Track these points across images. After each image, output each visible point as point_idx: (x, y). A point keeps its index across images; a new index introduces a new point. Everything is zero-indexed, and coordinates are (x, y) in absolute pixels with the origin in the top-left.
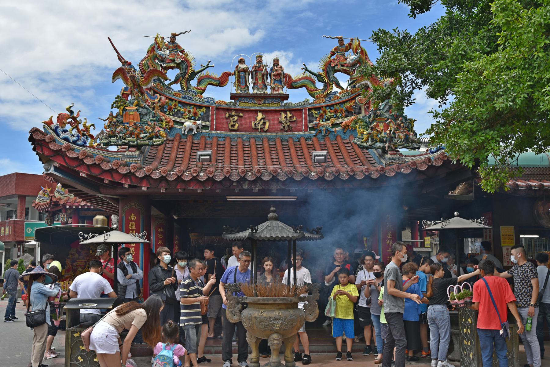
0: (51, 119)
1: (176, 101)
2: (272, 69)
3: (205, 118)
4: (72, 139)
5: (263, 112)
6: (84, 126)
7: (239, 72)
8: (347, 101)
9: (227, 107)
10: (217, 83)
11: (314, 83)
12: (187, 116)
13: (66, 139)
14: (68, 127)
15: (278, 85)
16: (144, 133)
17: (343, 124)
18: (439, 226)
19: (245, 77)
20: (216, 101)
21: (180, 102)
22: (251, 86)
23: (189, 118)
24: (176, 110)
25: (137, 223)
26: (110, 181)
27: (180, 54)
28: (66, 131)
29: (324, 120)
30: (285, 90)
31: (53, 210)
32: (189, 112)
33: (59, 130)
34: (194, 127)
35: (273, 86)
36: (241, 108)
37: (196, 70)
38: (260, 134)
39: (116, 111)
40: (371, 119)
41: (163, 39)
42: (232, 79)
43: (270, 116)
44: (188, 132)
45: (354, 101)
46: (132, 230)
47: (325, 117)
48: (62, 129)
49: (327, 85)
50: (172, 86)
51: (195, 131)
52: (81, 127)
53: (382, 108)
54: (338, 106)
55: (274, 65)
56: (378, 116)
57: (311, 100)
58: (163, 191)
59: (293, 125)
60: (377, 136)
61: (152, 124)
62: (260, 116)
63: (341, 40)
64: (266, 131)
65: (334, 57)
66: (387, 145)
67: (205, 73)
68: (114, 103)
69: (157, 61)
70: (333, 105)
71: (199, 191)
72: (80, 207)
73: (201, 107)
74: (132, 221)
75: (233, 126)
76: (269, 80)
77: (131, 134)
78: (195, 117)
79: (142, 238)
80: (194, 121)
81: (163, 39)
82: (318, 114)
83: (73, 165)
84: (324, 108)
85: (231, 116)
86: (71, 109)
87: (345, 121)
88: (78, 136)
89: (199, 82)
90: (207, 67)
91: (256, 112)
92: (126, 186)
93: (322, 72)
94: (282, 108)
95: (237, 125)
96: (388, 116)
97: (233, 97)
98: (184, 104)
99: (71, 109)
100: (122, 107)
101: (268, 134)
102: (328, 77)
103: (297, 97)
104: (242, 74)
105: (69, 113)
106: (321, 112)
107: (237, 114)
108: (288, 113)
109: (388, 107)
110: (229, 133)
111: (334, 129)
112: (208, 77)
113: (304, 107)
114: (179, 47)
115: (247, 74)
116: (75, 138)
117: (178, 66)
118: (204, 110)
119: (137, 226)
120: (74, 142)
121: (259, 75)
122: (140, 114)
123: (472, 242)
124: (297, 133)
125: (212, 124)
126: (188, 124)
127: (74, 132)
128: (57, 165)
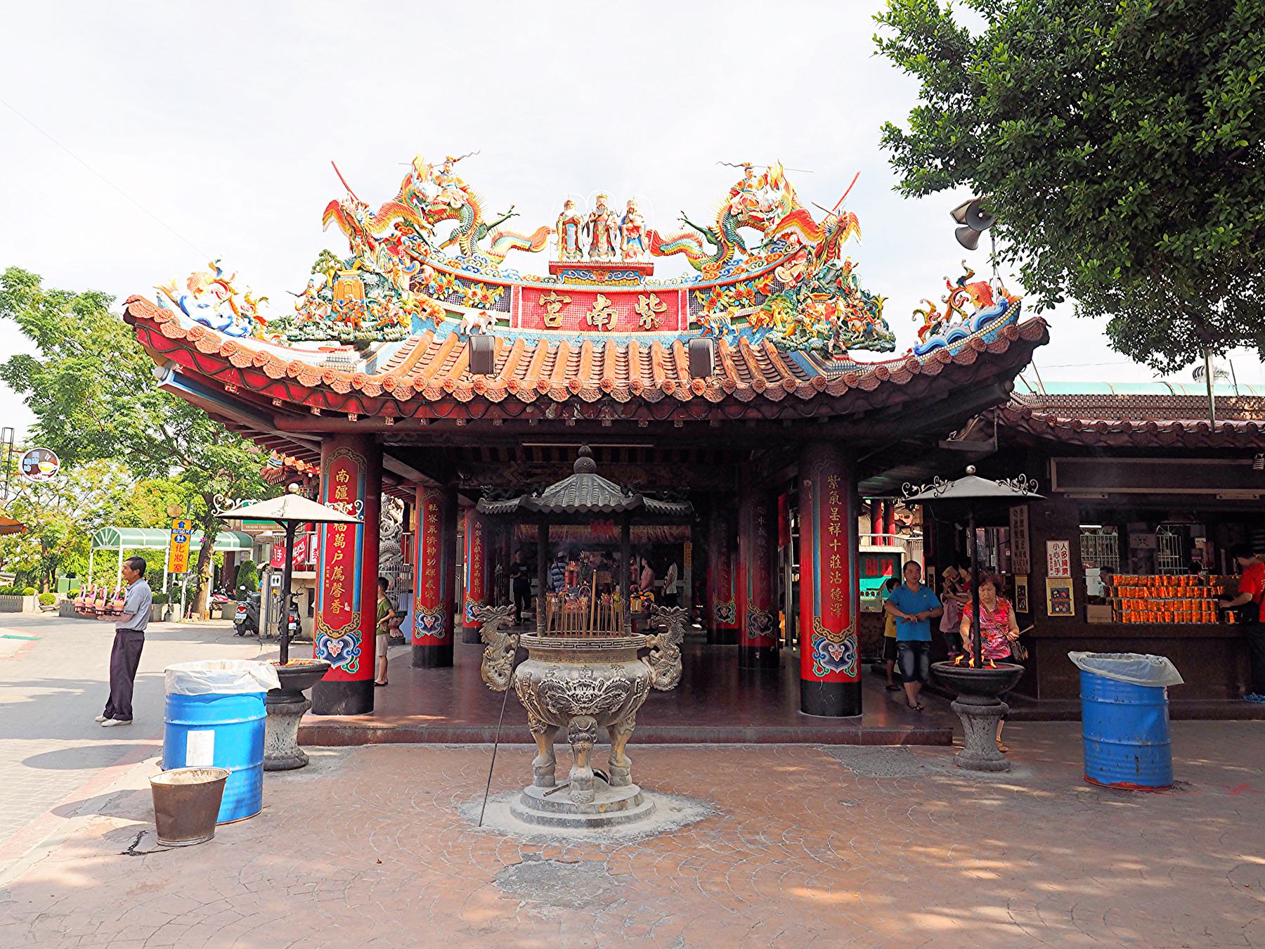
4: (216, 322)
18: (930, 495)
21: (457, 277)
25: (351, 486)
26: (284, 402)
32: (474, 294)
39: (320, 279)
40: (801, 298)
42: (554, 238)
45: (771, 277)
53: (821, 275)
55: (629, 212)
58: (389, 422)
62: (601, 301)
66: (831, 344)
69: (415, 201)
70: (733, 284)
71: (460, 423)
74: (340, 484)
77: (345, 320)
79: (350, 513)
89: (495, 241)
92: (316, 412)
97: (553, 269)
98: (466, 281)
100: (332, 273)
101: (615, 334)
103: (672, 272)
104: (571, 229)
109: (832, 273)
110: (546, 332)
111: (734, 327)
116: (224, 322)
117: (455, 214)
118: (501, 290)
120: (222, 329)
125: (516, 316)
127: (227, 310)
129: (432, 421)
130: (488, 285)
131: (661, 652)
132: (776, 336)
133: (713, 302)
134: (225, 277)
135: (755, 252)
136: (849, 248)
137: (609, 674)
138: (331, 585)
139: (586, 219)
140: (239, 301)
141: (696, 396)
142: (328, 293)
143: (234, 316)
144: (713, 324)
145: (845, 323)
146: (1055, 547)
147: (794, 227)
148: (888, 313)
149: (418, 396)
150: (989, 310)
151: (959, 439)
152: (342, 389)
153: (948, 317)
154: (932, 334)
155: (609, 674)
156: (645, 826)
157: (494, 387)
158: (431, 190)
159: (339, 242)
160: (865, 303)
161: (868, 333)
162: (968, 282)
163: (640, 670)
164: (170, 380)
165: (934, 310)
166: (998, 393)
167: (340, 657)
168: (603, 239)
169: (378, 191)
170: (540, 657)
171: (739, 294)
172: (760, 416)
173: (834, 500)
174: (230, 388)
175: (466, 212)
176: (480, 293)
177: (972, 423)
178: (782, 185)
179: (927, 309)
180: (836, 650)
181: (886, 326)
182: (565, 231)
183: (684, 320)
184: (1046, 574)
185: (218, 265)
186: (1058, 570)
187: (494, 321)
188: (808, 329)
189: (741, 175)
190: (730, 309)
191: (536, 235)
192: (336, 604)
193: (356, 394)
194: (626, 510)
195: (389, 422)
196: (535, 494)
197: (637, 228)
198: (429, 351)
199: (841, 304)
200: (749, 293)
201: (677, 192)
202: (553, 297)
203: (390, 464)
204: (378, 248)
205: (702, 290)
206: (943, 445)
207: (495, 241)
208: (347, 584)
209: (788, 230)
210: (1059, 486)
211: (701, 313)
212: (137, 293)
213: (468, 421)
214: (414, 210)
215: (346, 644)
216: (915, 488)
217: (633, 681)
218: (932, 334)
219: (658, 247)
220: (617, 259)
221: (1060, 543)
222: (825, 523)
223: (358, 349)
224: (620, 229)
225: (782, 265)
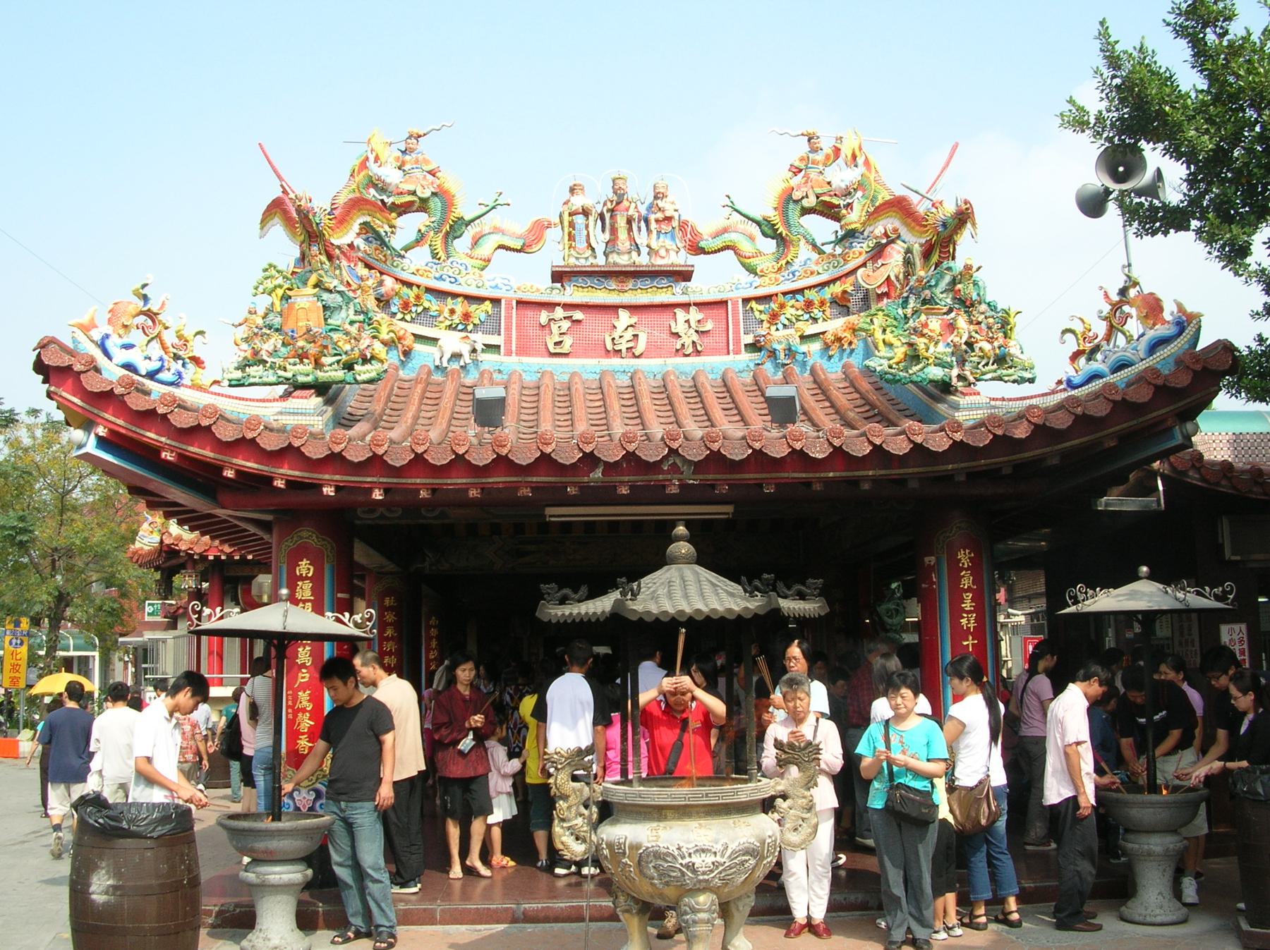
1: (418, 287)
2: (650, 208)
4: (144, 367)
8: (833, 281)
12: (448, 323)
13: (129, 367)
14: (136, 337)
16: (336, 355)
17: (829, 337)
19: (587, 226)
24: (420, 309)
25: (317, 581)
28: (128, 347)
29: (780, 326)
31: (168, 564)
32: (452, 312)
34: (465, 349)
39: (263, 302)
40: (909, 311)
45: (851, 279)
46: (304, 601)
47: (782, 318)
48: (121, 342)
51: (467, 358)
53: (933, 283)
54: (813, 291)
55: (656, 198)
61: (353, 330)
62: (625, 318)
66: (955, 372)
70: (800, 291)
72: (223, 557)
74: (302, 578)
77: (302, 356)
78: (466, 325)
80: (464, 334)
88: (161, 359)
97: (559, 277)
100: (280, 292)
102: (787, 224)
103: (715, 277)
104: (580, 219)
106: (774, 306)
107: (569, 314)
108: (693, 309)
109: (948, 279)
114: (427, 162)
115: (591, 219)
116: (155, 365)
117: (423, 205)
118: (487, 305)
119: (317, 591)
120: (151, 375)
121: (621, 222)
122: (325, 308)
123: (63, 650)
127: (155, 350)
128: (101, 431)
130: (470, 299)
131: (789, 802)
133: (774, 317)
134: (154, 306)
136: (966, 249)
138: (295, 716)
140: (170, 338)
141: (794, 450)
142: (277, 321)
143: (166, 357)
144: (776, 346)
146: (1231, 632)
150: (1161, 330)
154: (1089, 359)
158: (391, 175)
159: (283, 248)
164: (91, 447)
168: (622, 234)
171: (809, 304)
173: (967, 582)
175: (436, 204)
178: (860, 160)
179: (1079, 328)
182: (572, 225)
183: (737, 341)
185: (144, 292)
187: (479, 347)
190: (799, 325)
191: (530, 231)
197: (669, 219)
199: (962, 322)
200: (822, 303)
202: (559, 313)
205: (759, 299)
207: (476, 242)
212: (51, 334)
218: (1089, 359)
220: (643, 260)
221: (1236, 627)
222: (957, 613)
223: (319, 394)
224: (647, 221)
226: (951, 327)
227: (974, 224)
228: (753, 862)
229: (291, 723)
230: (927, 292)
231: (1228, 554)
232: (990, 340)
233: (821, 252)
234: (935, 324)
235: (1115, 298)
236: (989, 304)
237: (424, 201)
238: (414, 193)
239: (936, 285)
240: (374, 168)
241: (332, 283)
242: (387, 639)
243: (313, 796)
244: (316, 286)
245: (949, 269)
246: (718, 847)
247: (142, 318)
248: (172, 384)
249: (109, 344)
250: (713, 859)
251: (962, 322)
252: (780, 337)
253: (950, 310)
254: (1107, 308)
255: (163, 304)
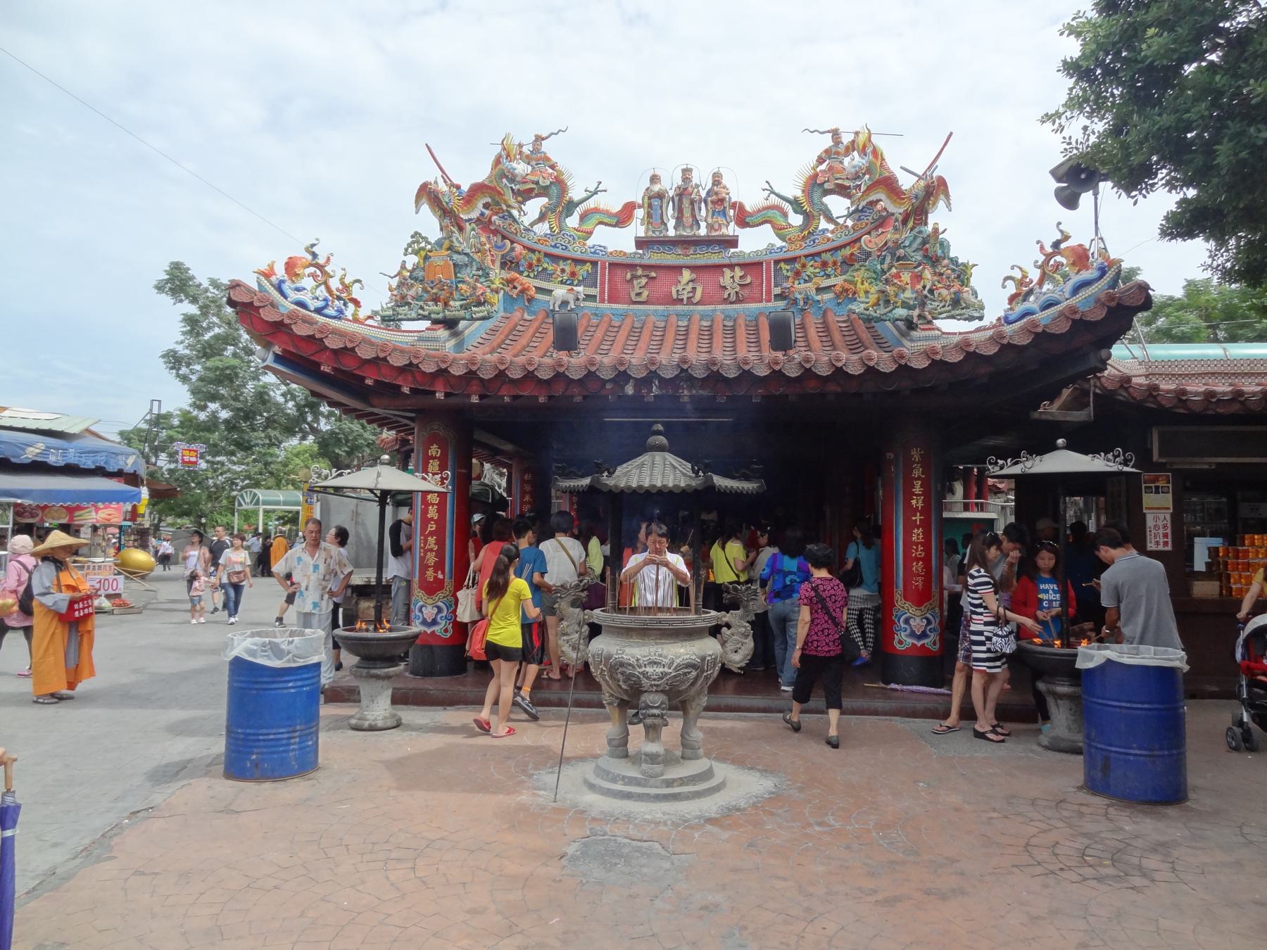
0: (271, 267)
3: (590, 281)
4: (313, 304)
5: (693, 268)
6: (342, 281)
7: (650, 198)
8: (844, 246)
9: (629, 261)
10: (614, 221)
11: (785, 215)
13: (301, 304)
14: (308, 283)
15: (721, 220)
17: (838, 289)
18: (1016, 470)
20: (610, 250)
21: (546, 255)
22: (671, 223)
23: (562, 282)
27: (550, 171)
30: (732, 230)
32: (563, 271)
33: (286, 287)
34: (571, 298)
35: (710, 220)
36: (653, 262)
37: (576, 198)
38: (686, 308)
39: (412, 260)
40: (885, 266)
41: (521, 146)
42: (639, 213)
43: (707, 276)
44: (560, 307)
45: (857, 245)
47: (804, 275)
49: (808, 217)
50: (536, 228)
52: (334, 284)
53: (907, 243)
55: (714, 184)
56: (899, 259)
57: (779, 243)
58: (475, 399)
59: (745, 292)
60: (896, 295)
62: (687, 275)
63: (835, 134)
64: (697, 304)
65: (823, 167)
66: (916, 312)
67: (591, 204)
68: (409, 245)
69: (504, 180)
70: (818, 254)
71: (542, 400)
73: (583, 262)
75: (639, 294)
76: (703, 212)
77: (436, 300)
81: (521, 146)
82: (791, 270)
83: (306, 352)
84: (803, 260)
85: (634, 277)
86: (314, 249)
87: (838, 281)
88: (325, 300)
89: (583, 217)
90: (596, 193)
91: (678, 269)
92: (406, 390)
93: (799, 194)
94: (726, 261)
95: (645, 293)
96: (919, 258)
97: (640, 243)
98: (555, 258)
99: (314, 249)
100: (423, 253)
101: (700, 308)
102: (811, 202)
103: (755, 241)
104: (656, 202)
105: (310, 257)
106: (797, 266)
107: (646, 273)
108: (737, 269)
109: (919, 240)
110: (632, 307)
111: (819, 298)
112: (596, 211)
113: (766, 258)
114: (548, 159)
115: (665, 201)
116: (320, 304)
117: (544, 191)
118: (588, 267)
120: (319, 311)
124: (753, 306)
126: (560, 292)
127: (322, 292)
128: (277, 350)
129: (515, 397)
130: (577, 261)
131: (732, 630)
132: (858, 308)
135: (841, 221)
136: (938, 217)
137: (683, 652)
139: (671, 193)
142: (420, 274)
145: (931, 291)
147: (880, 195)
148: (977, 280)
149: (501, 375)
150: (1086, 275)
151: (1051, 410)
152: (429, 368)
153: (1041, 283)
155: (683, 652)
156: (710, 806)
157: (575, 363)
158: (521, 168)
159: (430, 225)
160: (953, 270)
161: (956, 302)
162: (1063, 246)
163: (709, 647)
165: (1025, 277)
166: (1093, 362)
167: (434, 622)
168: (687, 213)
169: (471, 170)
170: (613, 633)
171: (825, 264)
172: (839, 390)
173: (917, 472)
174: (325, 368)
176: (568, 269)
177: (1066, 393)
178: (869, 150)
179: (1018, 275)
180: (918, 624)
181: (975, 294)
182: (650, 206)
183: (769, 292)
184: (1172, 515)
186: (1157, 543)
187: (582, 296)
188: (893, 299)
189: (827, 141)
192: (430, 573)
193: (442, 373)
194: (696, 490)
195: (475, 399)
196: (606, 474)
198: (519, 328)
199: (927, 274)
200: (835, 263)
201: (763, 166)
203: (479, 435)
204: (468, 227)
206: (1035, 415)
208: (440, 554)
209: (873, 197)
210: (1160, 455)
211: (785, 285)
213: (550, 397)
214: (497, 193)
215: (440, 610)
216: (1000, 462)
217: (703, 659)
218: (1024, 300)
219: (744, 219)
222: (909, 495)
225: (869, 233)
226: (918, 277)
227: (947, 196)
228: (694, 673)
229: (422, 559)
230: (902, 251)
231: (1155, 457)
232: (948, 287)
233: (836, 224)
234: (906, 277)
235: (1049, 250)
236: (951, 259)
237: (546, 188)
238: (537, 183)
239: (910, 246)
240: (506, 164)
241: (464, 247)
242: (525, 503)
243: (436, 610)
244: (449, 249)
245: (920, 232)
246: (666, 661)
247: (312, 269)
248: (334, 318)
249: (285, 287)
250: (662, 670)
251: (927, 274)
252: (801, 289)
253: (919, 265)
254: (1041, 258)
255: (328, 259)
